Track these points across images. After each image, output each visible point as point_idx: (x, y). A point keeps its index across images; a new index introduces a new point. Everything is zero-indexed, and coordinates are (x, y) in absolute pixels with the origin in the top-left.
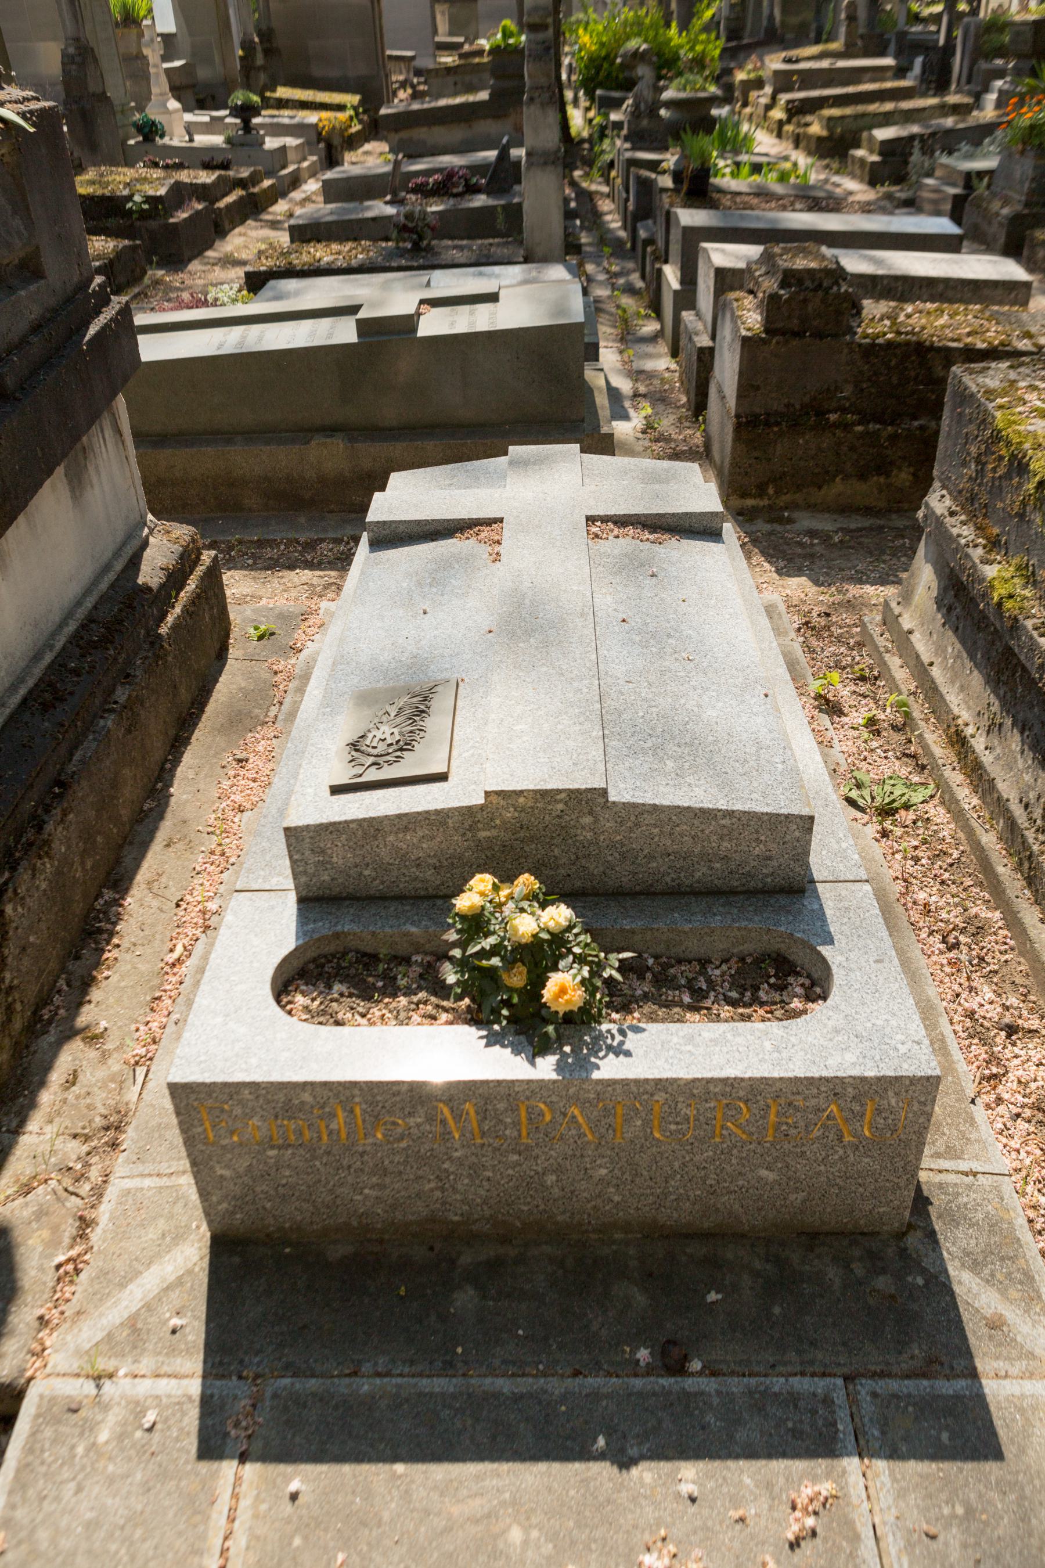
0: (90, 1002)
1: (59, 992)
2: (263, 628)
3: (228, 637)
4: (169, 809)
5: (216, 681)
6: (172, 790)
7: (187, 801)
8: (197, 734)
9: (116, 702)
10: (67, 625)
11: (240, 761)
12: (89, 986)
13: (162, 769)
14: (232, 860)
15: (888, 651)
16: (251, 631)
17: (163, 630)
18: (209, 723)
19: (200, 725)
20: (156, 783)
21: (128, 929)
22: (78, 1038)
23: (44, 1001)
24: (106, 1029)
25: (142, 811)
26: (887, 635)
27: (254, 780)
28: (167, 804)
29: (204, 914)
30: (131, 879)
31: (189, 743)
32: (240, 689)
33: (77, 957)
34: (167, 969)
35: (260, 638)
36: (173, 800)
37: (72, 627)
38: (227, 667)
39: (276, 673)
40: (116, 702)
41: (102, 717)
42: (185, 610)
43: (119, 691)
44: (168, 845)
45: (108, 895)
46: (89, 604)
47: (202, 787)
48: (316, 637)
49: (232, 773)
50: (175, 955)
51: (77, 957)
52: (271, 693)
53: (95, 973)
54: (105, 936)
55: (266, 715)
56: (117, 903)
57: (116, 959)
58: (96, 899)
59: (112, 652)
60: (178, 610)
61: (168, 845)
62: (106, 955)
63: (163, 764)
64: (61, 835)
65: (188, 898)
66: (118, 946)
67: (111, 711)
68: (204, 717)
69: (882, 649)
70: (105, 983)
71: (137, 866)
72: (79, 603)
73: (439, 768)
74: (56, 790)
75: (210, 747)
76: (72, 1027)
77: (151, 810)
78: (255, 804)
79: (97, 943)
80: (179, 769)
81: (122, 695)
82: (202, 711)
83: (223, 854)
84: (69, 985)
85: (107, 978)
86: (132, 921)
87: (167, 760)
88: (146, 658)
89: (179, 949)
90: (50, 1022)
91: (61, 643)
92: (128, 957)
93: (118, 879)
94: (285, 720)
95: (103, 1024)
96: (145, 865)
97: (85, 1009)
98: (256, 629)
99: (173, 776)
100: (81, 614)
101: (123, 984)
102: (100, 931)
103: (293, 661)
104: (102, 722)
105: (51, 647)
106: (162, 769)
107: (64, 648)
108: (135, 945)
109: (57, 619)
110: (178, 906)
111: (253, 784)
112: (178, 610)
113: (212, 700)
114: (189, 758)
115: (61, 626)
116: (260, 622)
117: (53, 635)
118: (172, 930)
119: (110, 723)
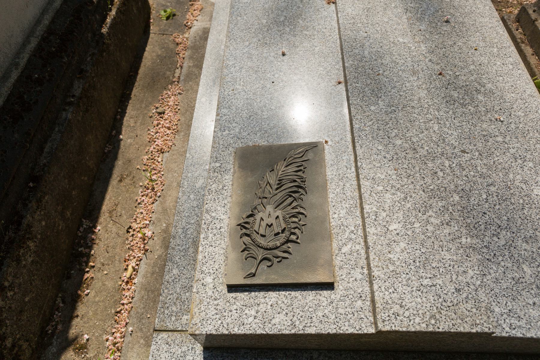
0: (77, 316)
1: (57, 310)
2: (169, 10)
3: (149, 18)
4: (120, 150)
5: (144, 50)
6: (121, 137)
7: (131, 144)
8: (135, 91)
9: (73, 96)
10: (29, 43)
11: (160, 113)
12: (76, 302)
13: (115, 119)
14: (159, 194)
15: (523, 42)
16: (162, 13)
17: (104, 30)
18: (141, 83)
19: (136, 84)
20: (112, 130)
21: (99, 252)
22: (71, 349)
23: (48, 320)
24: (88, 340)
25: (105, 153)
26: (520, 30)
27: (169, 128)
28: (118, 147)
29: (144, 240)
30: (100, 208)
31: (130, 98)
32: (158, 56)
33: (69, 277)
34: (124, 285)
35: (168, 18)
36: (122, 143)
37: (33, 43)
38: (150, 40)
39: (178, 44)
40: (73, 96)
41: (65, 110)
42: (119, 11)
43: (76, 83)
44: (120, 181)
45: (86, 223)
46: (46, 21)
47: (139, 133)
48: (199, 18)
49: (155, 122)
50: (128, 274)
51: (69, 277)
52: (175, 59)
53: (79, 292)
54: (85, 259)
55: (174, 77)
56: (91, 229)
57: (92, 278)
58: (78, 229)
59: (66, 59)
60: (113, 12)
61: (120, 181)
62: (87, 276)
63: (116, 115)
64: (36, 220)
65: (135, 225)
66: (93, 267)
67: (70, 104)
68: (139, 77)
69: (519, 40)
70: (86, 298)
71: (103, 198)
72: (38, 22)
73: (322, 277)
74: (31, 184)
75: (142, 101)
76: (67, 338)
77: (109, 152)
78: (170, 147)
79: (80, 264)
80: (125, 119)
81: (78, 89)
82: (137, 73)
83: (153, 189)
84: (64, 302)
85: (87, 295)
86: (101, 244)
87: (118, 112)
88: (93, 54)
89: (130, 269)
90: (53, 334)
91: (25, 60)
92: (99, 275)
93: (91, 211)
94: (185, 80)
95: (86, 336)
96: (108, 197)
97: (75, 321)
98: (165, 11)
99: (122, 124)
100: (40, 31)
101: (97, 299)
102: (82, 255)
103: (186, 35)
104: (64, 114)
105: (17, 65)
106: (115, 119)
107: (29, 61)
108: (103, 265)
109: (20, 40)
110: (128, 232)
111: (168, 132)
112: (113, 12)
113: (142, 65)
114: (130, 111)
115: (24, 45)
116: (167, 7)
117: (18, 54)
118: (126, 252)
119: (70, 116)
